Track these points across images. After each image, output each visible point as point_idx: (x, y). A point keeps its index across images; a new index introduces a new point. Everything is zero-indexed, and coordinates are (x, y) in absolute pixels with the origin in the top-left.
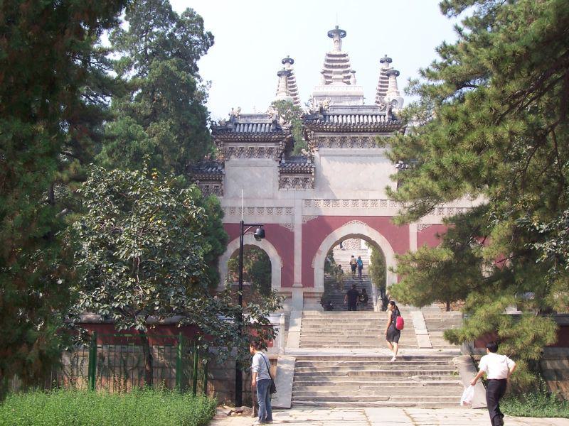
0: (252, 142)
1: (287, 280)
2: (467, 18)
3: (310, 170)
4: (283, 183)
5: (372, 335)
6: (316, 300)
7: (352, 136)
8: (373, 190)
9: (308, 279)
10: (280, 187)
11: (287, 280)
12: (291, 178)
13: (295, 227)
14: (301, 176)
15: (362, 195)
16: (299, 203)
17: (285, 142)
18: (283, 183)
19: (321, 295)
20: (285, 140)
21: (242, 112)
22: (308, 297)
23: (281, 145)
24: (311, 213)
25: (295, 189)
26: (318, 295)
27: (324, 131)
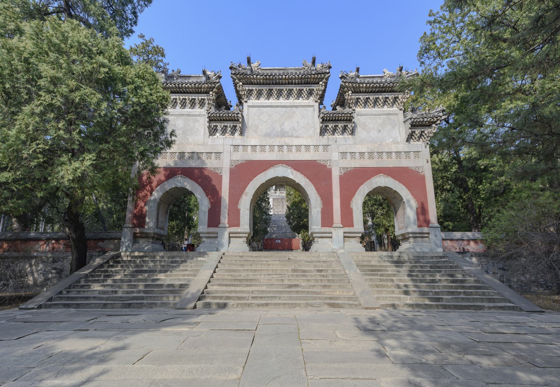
0: (184, 93)
1: (327, 220)
2: (288, 207)
3: (237, 117)
4: (212, 131)
5: (296, 283)
6: (242, 240)
7: (278, 88)
8: (297, 137)
9: (347, 220)
10: (211, 134)
11: (327, 220)
12: (220, 125)
13: (223, 171)
14: (230, 124)
15: (288, 141)
16: (229, 148)
17: (214, 92)
18: (212, 131)
19: (247, 235)
20: (215, 90)
21: (182, 74)
22: (233, 237)
23: (212, 95)
24: (240, 156)
25: (224, 137)
26: (244, 235)
27: (252, 84)
